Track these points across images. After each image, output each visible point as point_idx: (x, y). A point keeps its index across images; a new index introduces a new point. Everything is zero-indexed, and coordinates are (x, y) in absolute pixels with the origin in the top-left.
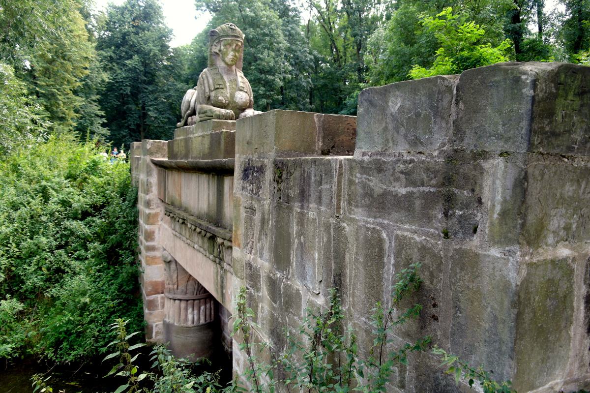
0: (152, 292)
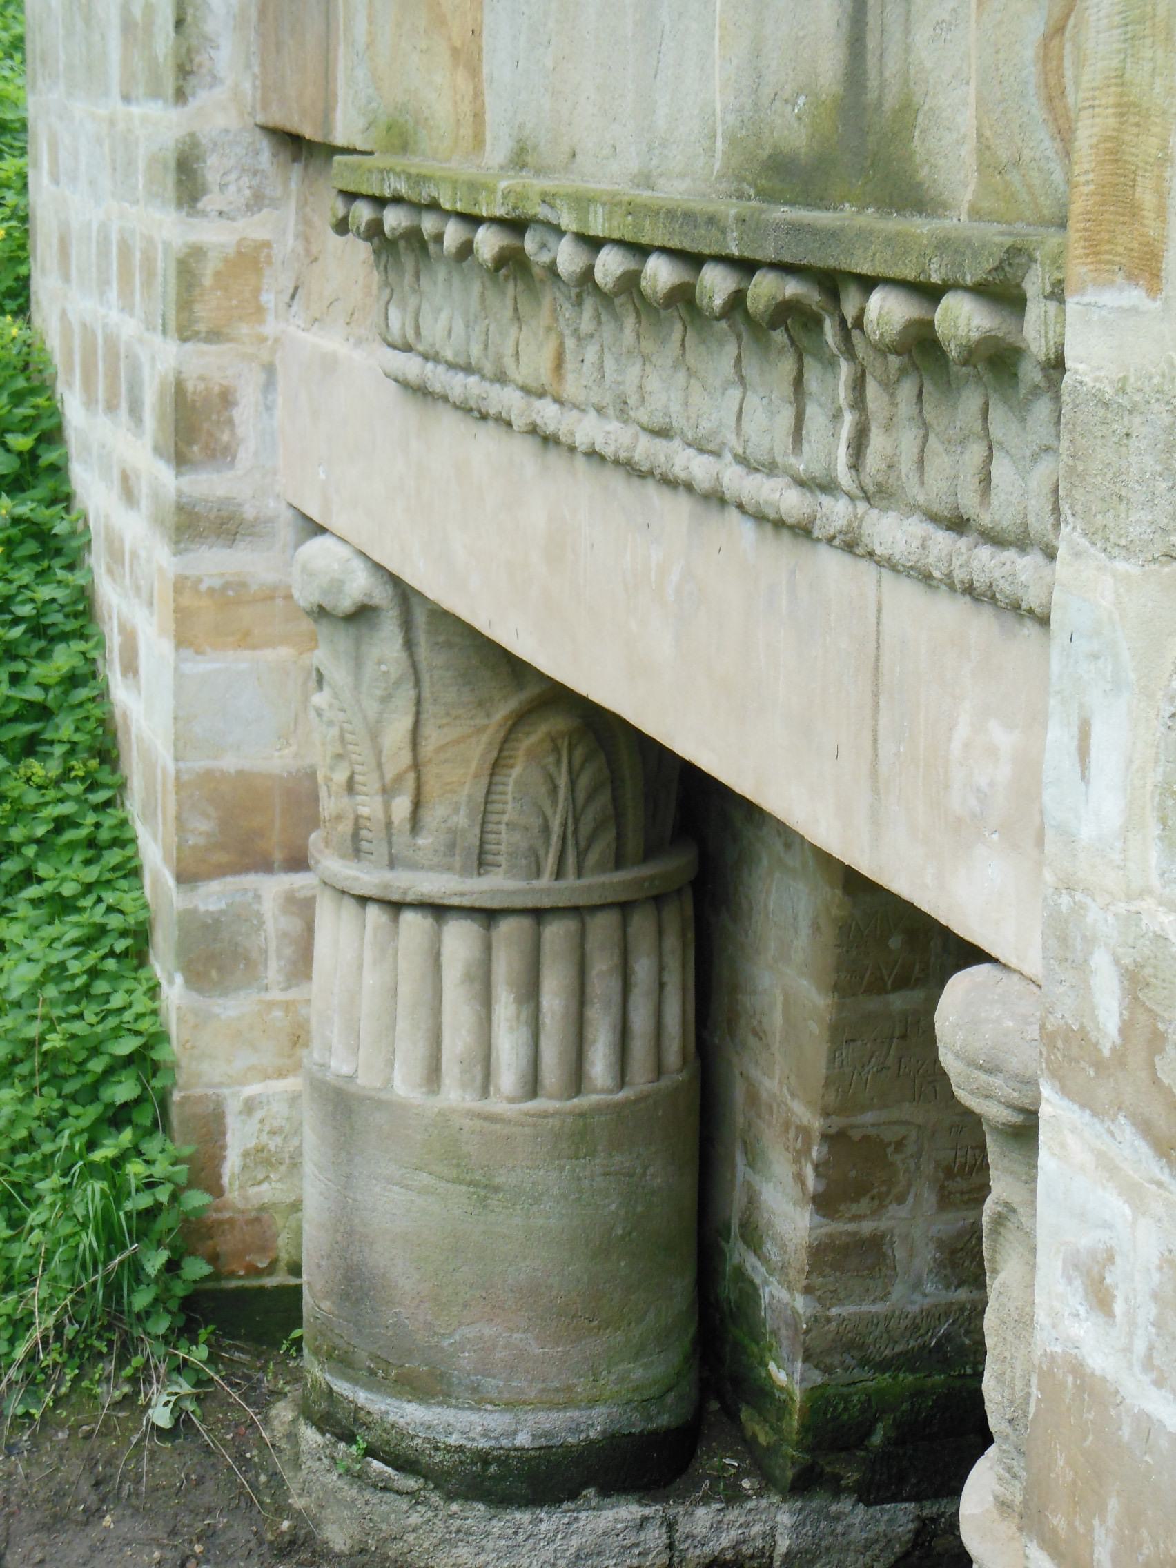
0: (221, 857)
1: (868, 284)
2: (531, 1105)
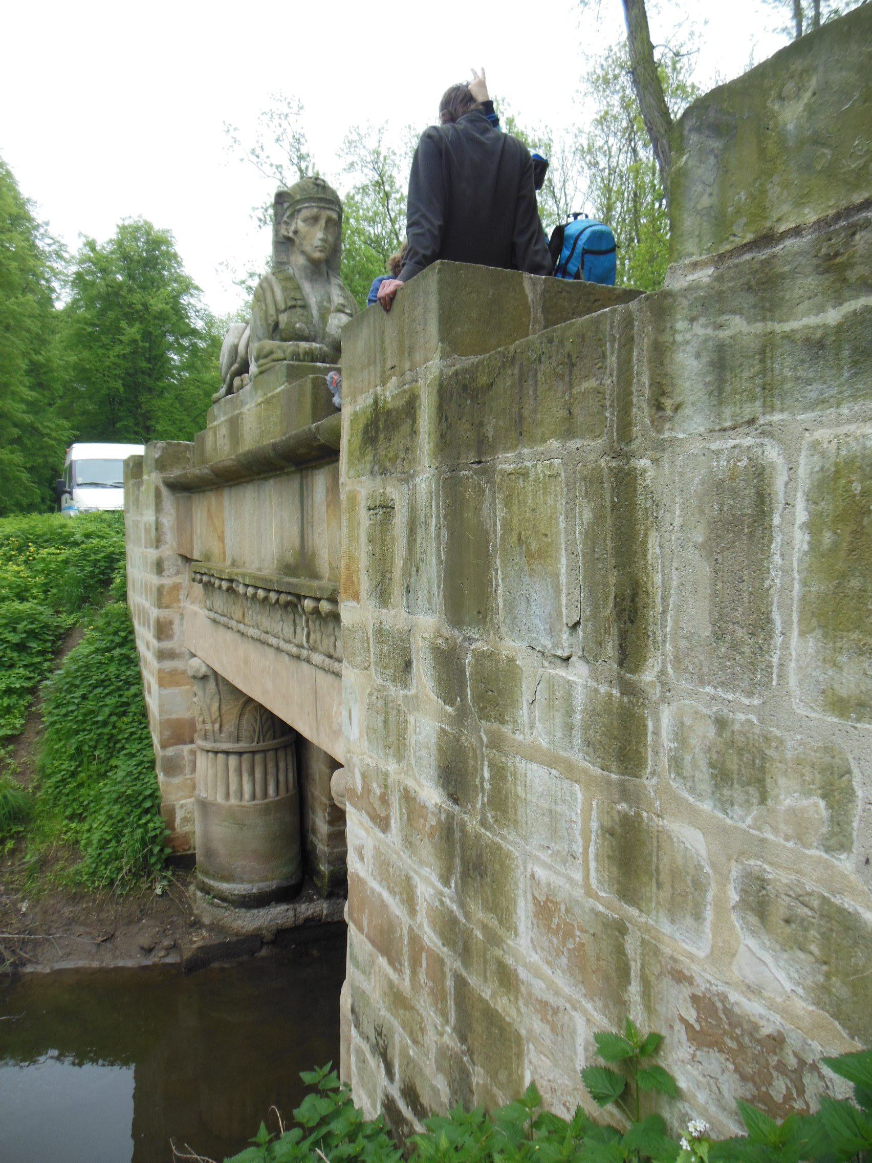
0: (173, 741)
1: (306, 597)
2: (253, 802)
